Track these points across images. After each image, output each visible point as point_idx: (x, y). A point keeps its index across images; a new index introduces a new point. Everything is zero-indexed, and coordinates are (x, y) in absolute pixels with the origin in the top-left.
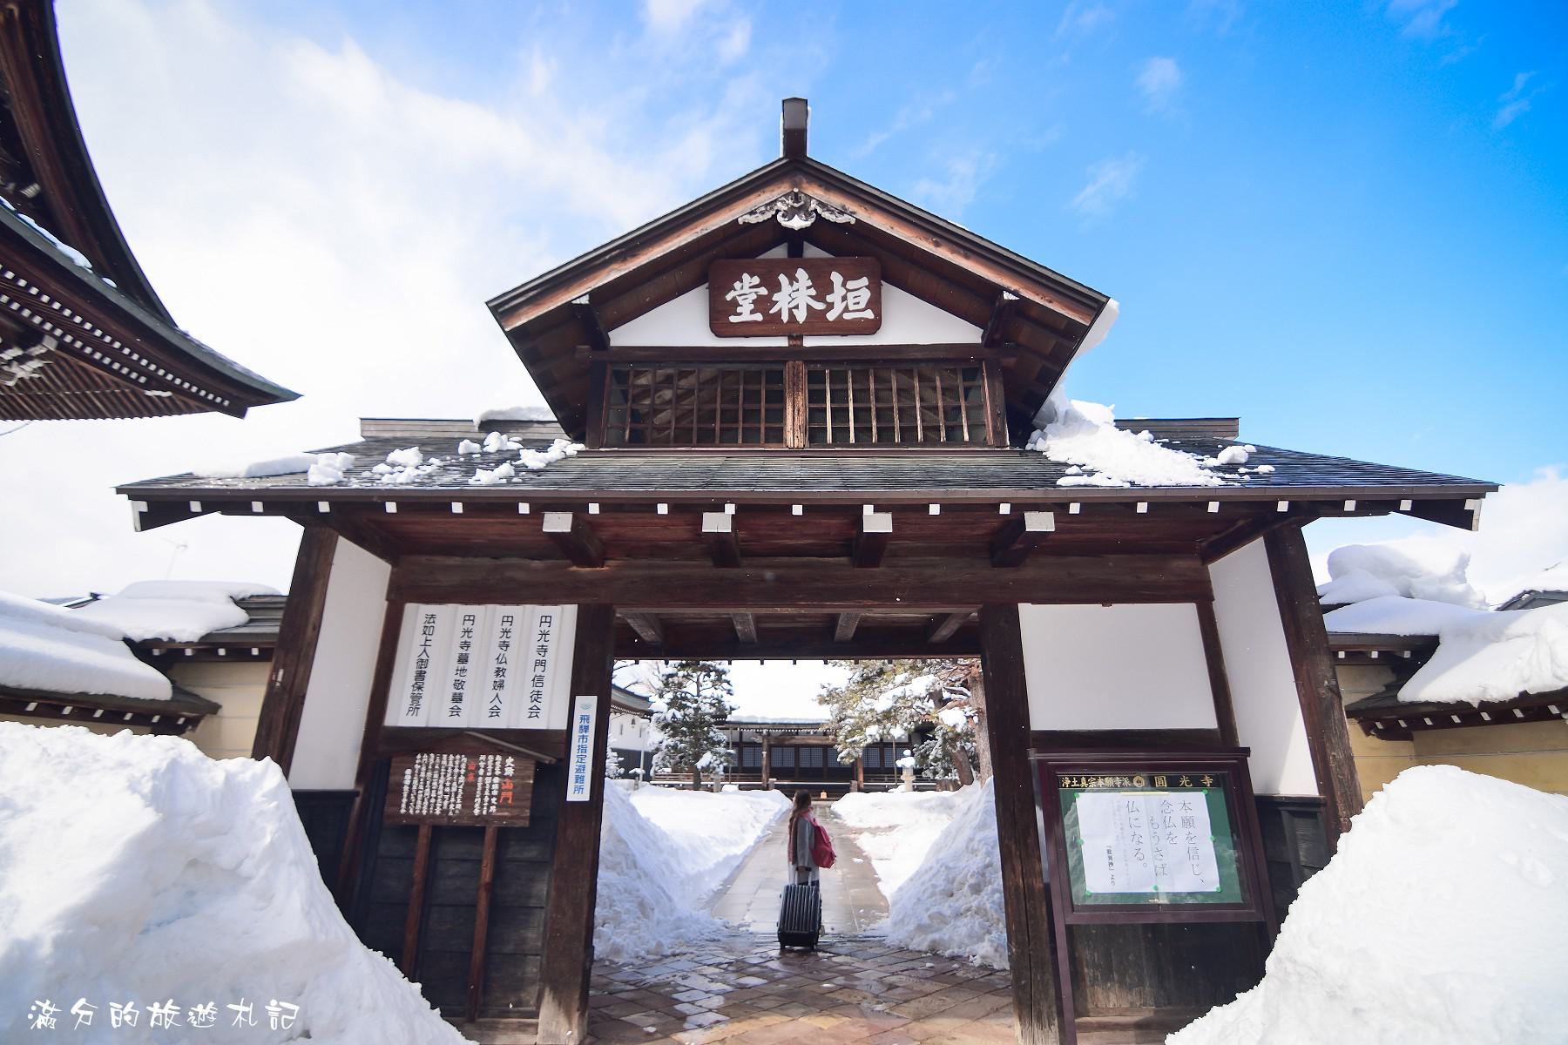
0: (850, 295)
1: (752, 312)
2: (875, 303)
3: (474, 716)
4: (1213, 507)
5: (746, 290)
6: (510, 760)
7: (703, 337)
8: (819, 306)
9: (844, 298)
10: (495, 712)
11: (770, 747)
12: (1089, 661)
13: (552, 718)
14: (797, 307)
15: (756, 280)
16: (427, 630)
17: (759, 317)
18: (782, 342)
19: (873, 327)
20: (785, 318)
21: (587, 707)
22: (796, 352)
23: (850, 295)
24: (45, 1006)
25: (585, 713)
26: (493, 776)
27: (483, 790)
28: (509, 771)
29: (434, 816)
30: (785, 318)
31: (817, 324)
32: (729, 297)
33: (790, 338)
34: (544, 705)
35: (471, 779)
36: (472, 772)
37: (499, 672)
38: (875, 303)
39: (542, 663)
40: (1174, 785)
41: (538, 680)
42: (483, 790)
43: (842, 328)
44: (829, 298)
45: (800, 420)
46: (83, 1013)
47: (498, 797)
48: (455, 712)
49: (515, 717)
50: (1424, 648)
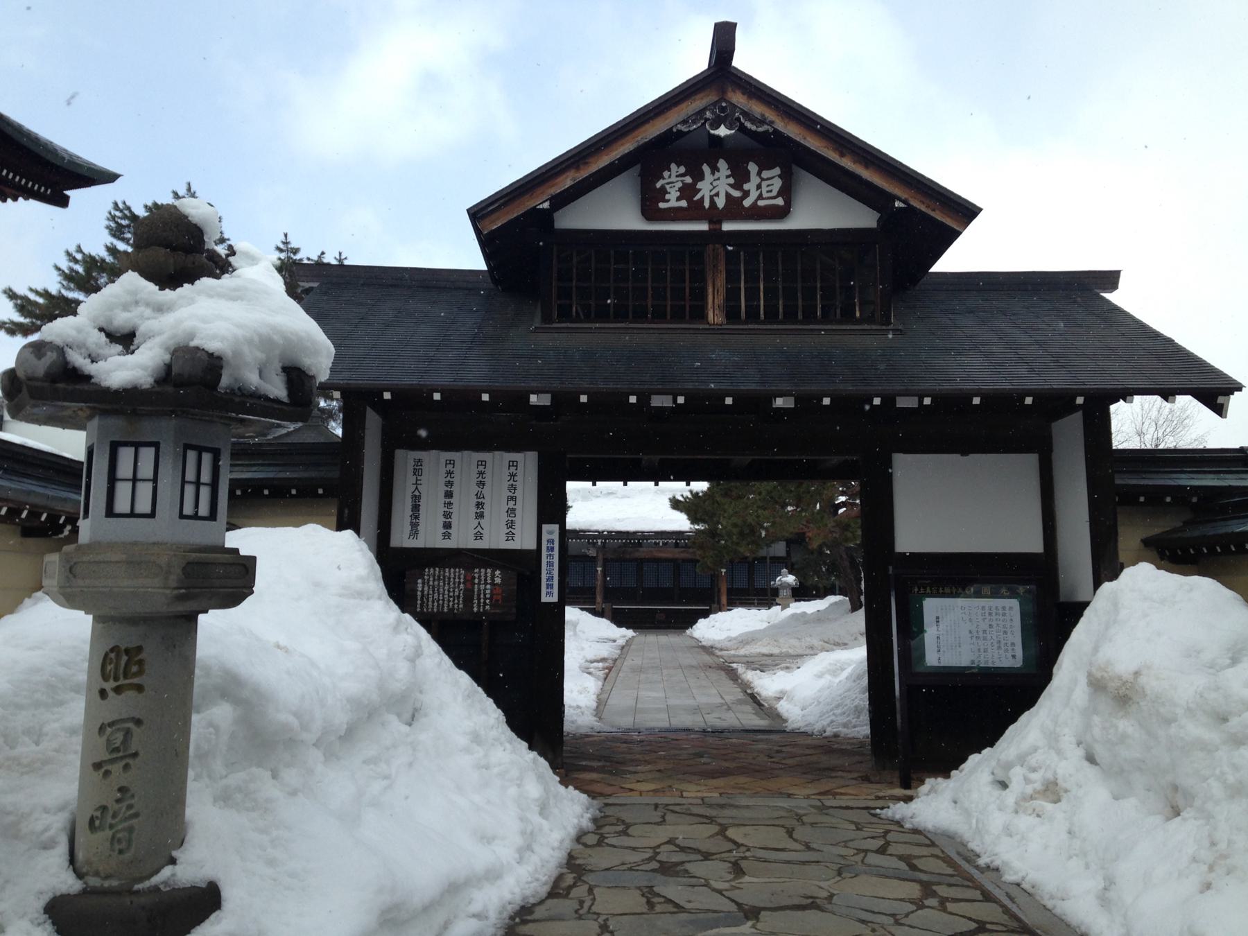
0: (764, 184)
1: (678, 199)
3: (462, 538)
4: (1029, 401)
5: (673, 180)
6: (498, 573)
8: (736, 194)
9: (759, 187)
10: (479, 536)
11: (605, 561)
12: (940, 504)
13: (524, 540)
14: (717, 195)
15: (682, 170)
16: (417, 472)
17: (684, 203)
18: (703, 227)
19: (781, 213)
20: (707, 204)
21: (551, 533)
23: (764, 184)
25: (550, 537)
26: (486, 583)
27: (479, 595)
28: (498, 580)
29: (443, 612)
30: (707, 204)
31: (735, 209)
32: (658, 185)
33: (711, 222)
34: (517, 530)
35: (469, 586)
36: (469, 581)
37: (479, 505)
39: (513, 498)
41: (512, 512)
42: (479, 595)
44: (746, 187)
45: (720, 300)
47: (491, 599)
48: (447, 536)
49: (495, 539)
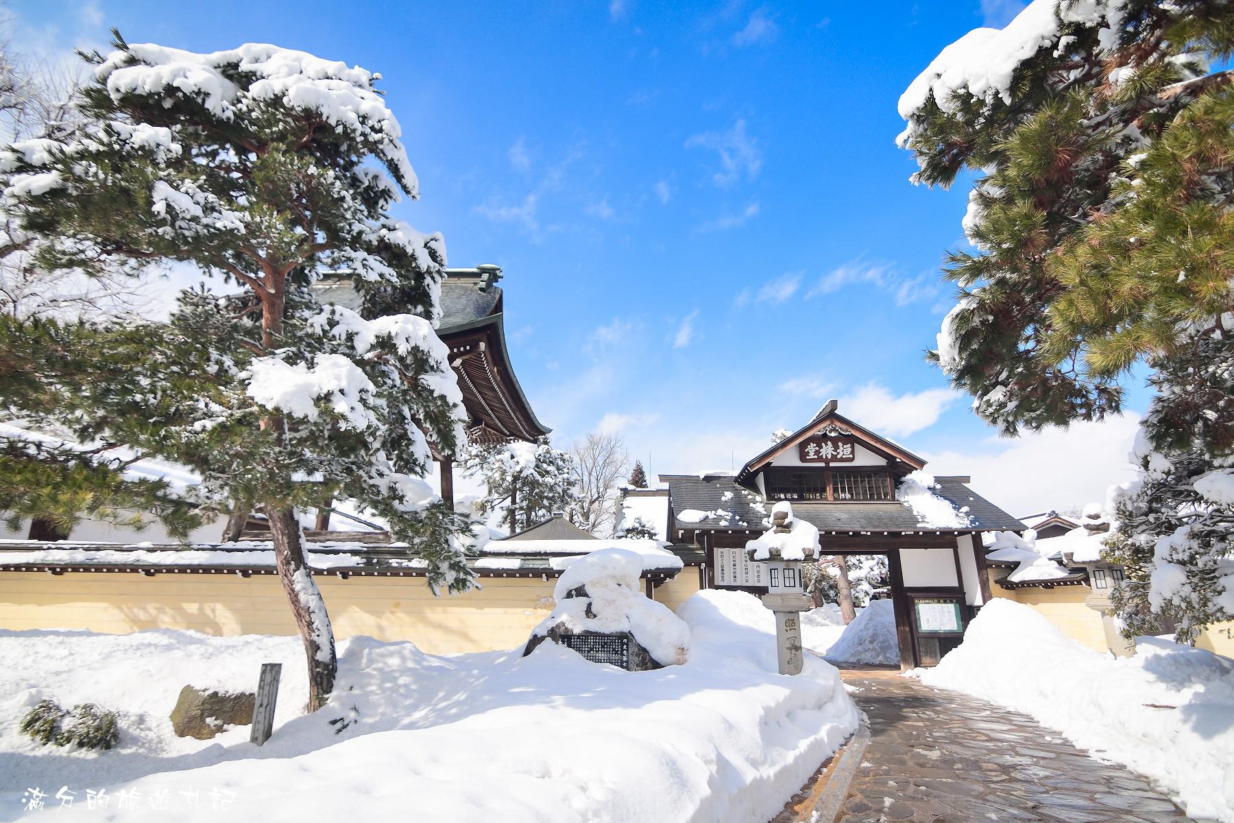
2: (853, 452)
7: (796, 462)
12: (919, 567)
18: (823, 465)
22: (827, 468)
24: (36, 792)
31: (834, 458)
38: (853, 452)
40: (945, 602)
43: (842, 460)
46: (65, 798)
50: (1017, 564)
